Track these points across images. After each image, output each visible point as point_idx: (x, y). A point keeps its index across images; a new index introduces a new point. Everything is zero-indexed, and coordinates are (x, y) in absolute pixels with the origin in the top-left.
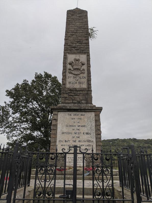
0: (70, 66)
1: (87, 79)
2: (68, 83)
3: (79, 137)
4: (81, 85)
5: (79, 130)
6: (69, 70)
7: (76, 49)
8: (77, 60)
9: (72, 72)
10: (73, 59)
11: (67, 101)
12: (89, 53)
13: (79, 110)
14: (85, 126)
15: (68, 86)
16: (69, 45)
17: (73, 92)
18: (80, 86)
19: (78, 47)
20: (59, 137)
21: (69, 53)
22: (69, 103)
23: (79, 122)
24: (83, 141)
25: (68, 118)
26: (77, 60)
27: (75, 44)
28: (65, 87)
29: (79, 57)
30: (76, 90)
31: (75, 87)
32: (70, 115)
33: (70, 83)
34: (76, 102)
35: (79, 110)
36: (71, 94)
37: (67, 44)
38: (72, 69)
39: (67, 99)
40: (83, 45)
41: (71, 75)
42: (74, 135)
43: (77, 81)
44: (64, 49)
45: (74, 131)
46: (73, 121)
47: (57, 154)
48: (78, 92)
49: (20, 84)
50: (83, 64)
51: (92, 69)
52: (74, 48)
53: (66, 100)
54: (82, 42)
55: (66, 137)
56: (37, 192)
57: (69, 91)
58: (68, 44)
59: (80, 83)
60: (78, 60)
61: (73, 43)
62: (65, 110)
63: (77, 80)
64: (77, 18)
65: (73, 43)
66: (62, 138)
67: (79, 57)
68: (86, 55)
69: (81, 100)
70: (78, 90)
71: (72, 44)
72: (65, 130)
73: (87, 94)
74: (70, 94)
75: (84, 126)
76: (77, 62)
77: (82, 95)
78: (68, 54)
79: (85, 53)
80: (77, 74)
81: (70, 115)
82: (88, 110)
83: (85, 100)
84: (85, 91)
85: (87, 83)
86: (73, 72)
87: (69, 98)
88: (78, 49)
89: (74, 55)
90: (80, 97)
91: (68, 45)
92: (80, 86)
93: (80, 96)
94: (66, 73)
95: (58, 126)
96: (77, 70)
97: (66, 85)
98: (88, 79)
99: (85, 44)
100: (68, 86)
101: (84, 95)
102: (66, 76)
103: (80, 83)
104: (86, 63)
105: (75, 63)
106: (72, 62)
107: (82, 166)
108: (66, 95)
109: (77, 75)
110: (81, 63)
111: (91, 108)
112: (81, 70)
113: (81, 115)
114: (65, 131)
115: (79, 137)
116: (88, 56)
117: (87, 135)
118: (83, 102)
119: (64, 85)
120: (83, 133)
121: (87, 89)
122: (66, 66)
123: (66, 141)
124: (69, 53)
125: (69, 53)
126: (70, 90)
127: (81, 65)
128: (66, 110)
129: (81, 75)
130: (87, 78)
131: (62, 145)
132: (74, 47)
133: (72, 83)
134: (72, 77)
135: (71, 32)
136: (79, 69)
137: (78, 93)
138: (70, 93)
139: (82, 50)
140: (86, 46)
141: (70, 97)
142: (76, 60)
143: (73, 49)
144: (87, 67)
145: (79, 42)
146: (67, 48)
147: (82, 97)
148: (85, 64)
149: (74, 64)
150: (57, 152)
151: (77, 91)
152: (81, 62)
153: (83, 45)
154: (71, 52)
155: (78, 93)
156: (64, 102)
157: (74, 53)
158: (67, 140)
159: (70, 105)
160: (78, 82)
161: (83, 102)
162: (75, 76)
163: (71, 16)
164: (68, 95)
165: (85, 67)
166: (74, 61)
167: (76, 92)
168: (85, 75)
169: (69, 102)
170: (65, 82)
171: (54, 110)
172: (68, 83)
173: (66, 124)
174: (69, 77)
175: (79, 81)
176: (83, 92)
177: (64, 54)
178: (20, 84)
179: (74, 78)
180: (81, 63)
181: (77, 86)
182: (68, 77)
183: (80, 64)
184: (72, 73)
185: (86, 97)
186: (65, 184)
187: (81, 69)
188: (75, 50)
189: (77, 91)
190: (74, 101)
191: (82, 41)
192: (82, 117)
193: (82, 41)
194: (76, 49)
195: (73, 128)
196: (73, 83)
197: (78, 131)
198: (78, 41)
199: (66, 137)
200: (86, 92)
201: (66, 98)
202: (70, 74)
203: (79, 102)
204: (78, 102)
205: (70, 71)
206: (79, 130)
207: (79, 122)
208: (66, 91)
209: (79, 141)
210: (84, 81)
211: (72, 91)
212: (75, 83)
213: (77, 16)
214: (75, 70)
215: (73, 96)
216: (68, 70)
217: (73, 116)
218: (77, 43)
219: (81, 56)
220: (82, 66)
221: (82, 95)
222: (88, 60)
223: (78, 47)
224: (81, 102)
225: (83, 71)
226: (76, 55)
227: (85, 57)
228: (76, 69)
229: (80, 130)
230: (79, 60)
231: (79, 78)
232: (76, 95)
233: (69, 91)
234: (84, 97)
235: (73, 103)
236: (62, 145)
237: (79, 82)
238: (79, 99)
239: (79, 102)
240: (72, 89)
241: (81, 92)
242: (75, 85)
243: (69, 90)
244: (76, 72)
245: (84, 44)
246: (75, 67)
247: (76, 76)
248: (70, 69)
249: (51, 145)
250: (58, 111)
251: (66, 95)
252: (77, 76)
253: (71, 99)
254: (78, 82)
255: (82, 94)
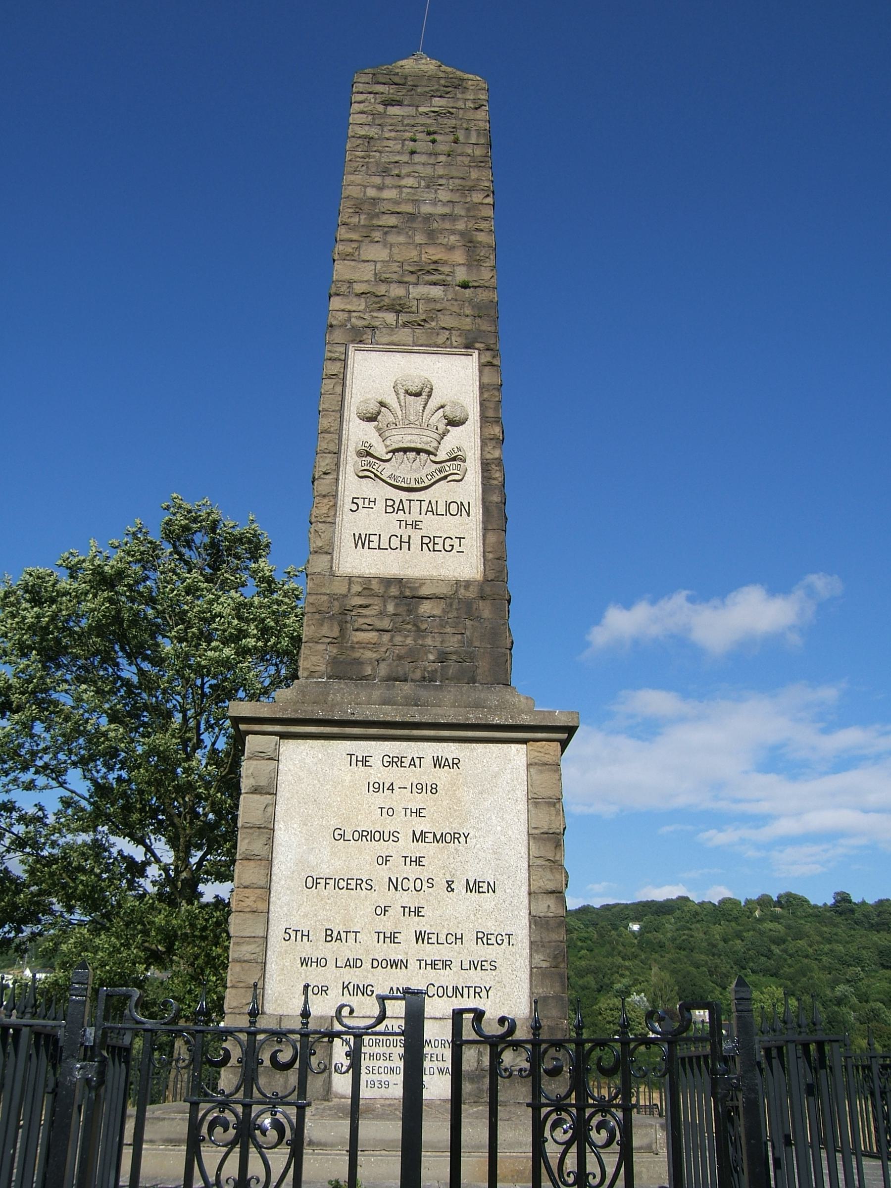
3: (418, 912)
5: (418, 861)
8: (418, 394)
9: (379, 467)
14: (462, 839)
20: (289, 905)
23: (418, 813)
24: (442, 939)
25: (347, 784)
32: (365, 761)
33: (361, 541)
38: (380, 450)
42: (382, 895)
43: (410, 531)
45: (382, 874)
46: (381, 799)
47: (252, 1034)
49: (829, 904)
52: (398, 312)
55: (334, 908)
56: (232, 1144)
60: (422, 392)
63: (415, 525)
64: (422, 120)
66: (305, 915)
72: (331, 860)
75: (455, 837)
81: (365, 761)
95: (281, 835)
106: (382, 404)
112: (442, 455)
113: (438, 763)
114: (325, 871)
115: (418, 912)
117: (474, 895)
120: (449, 884)
123: (335, 935)
127: (442, 427)
129: (440, 493)
131: (304, 962)
134: (381, 504)
136: (428, 453)
149: (391, 419)
150: (253, 1023)
157: (394, 347)
158: (341, 928)
163: (381, 108)
171: (257, 728)
173: (334, 822)
174: (360, 502)
178: (829, 904)
179: (393, 507)
182: (349, 505)
187: (437, 449)
192: (442, 776)
194: (403, 318)
195: (383, 848)
197: (413, 871)
199: (334, 908)
206: (418, 861)
207: (418, 813)
209: (420, 937)
212: (395, 542)
213: (421, 109)
217: (378, 772)
218: (412, 279)
225: (450, 467)
228: (405, 450)
229: (424, 861)
236: (304, 962)
237: (426, 540)
244: (408, 470)
246: (400, 439)
247: (404, 495)
249: (238, 961)
250: (284, 736)
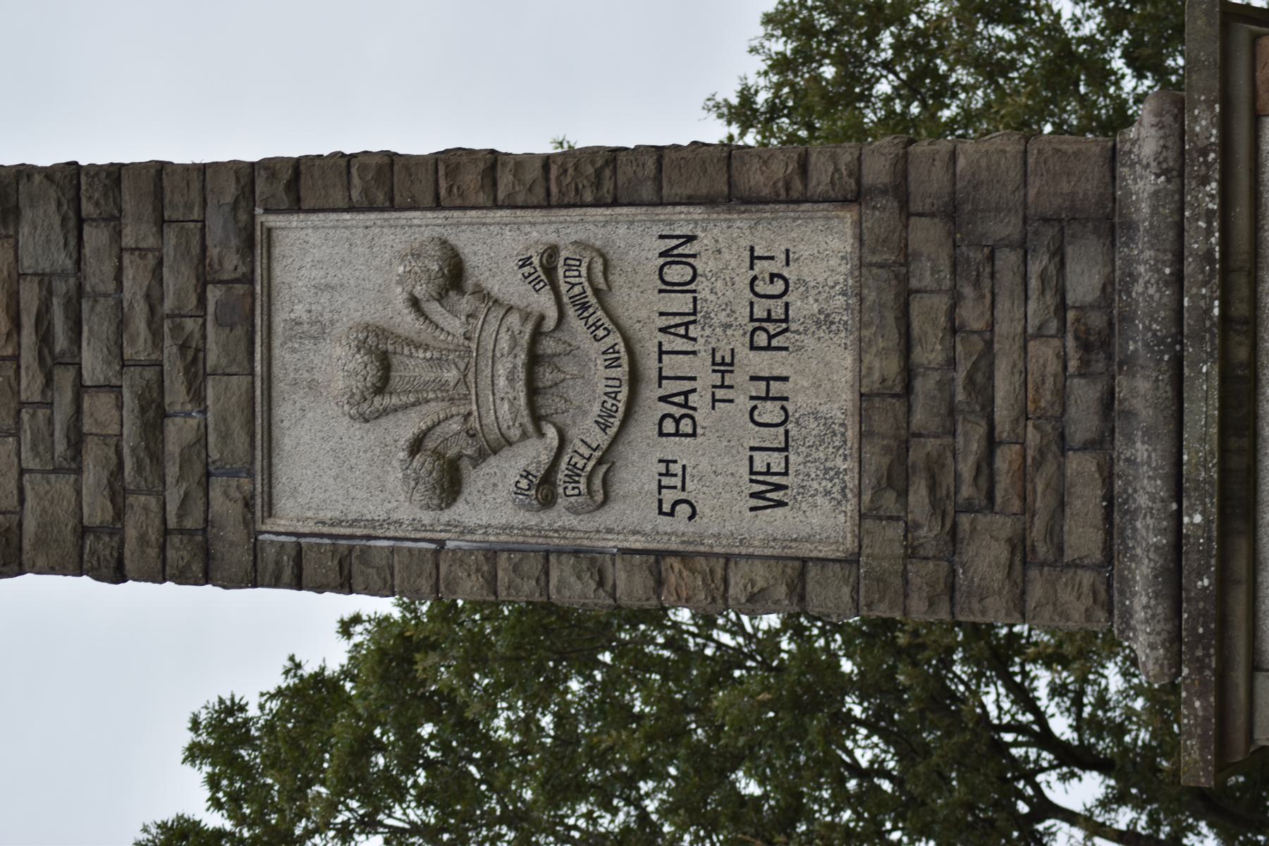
0: (475, 479)
1: (697, 212)
2: (777, 522)
4: (802, 307)
6: (548, 502)
7: (177, 393)
8: (385, 363)
10: (358, 437)
11: (1083, 537)
12: (247, 176)
13: (1242, 354)
15: (820, 518)
16: (117, 493)
17: (931, 445)
18: (824, 321)
19: (139, 346)
21: (255, 506)
22: (1109, 498)
26: (385, 363)
27: (99, 409)
28: (852, 560)
29: (319, 331)
30: (886, 400)
31: (840, 404)
33: (768, 494)
34: (1084, 395)
35: (1242, 354)
36: (966, 469)
37: (83, 531)
39: (1039, 524)
40: (108, 268)
41: (638, 473)
43: (738, 377)
44: (182, 578)
48: (930, 353)
50: (454, 275)
51: (525, 136)
52: (163, 415)
53: (1060, 549)
54: (45, 280)
57: (919, 495)
58: (97, 510)
59: (770, 329)
61: (77, 441)
62: (1240, 566)
63: (724, 366)
65: (77, 441)
67: (319, 331)
68: (295, 220)
69: (1062, 307)
70: (892, 366)
71: (93, 456)
73: (952, 212)
74: (966, 491)
76: (411, 368)
77: (968, 291)
78: (282, 524)
79: (251, 242)
80: (622, 372)
82: (1241, 211)
83: (1059, 255)
84: (906, 256)
85: (767, 212)
86: (588, 433)
87: (1027, 509)
88: (183, 347)
89: (283, 411)
90: (1002, 328)
91: (119, 514)
92: (824, 321)
93: (991, 326)
94: (612, 543)
96: (547, 376)
97: (805, 550)
98: (709, 201)
99: (95, 237)
100: (820, 518)
101: (972, 265)
102: (660, 555)
103: (770, 329)
104: (424, 226)
105: (435, 410)
106: (416, 446)
107: (86, 228)
108: (986, 556)
109: (635, 378)
110: (433, 308)
111: (1205, 181)
112: (544, 302)
116: (298, 183)
118: (1084, 282)
119: (813, 572)
121: (882, 215)
122: (491, 554)
124: (248, 504)
125: (248, 504)
126: (896, 479)
127: (465, 303)
128: (1241, 545)
129: (640, 304)
130: (684, 219)
132: (154, 416)
133: (777, 461)
134: (671, 448)
135: (238, 383)
136: (537, 334)
137: (952, 362)
138: (947, 481)
139: (202, 284)
140: (114, 220)
141: (1004, 482)
142: (382, 386)
143: (178, 433)
144: (496, 206)
145: (61, 342)
146: (166, 532)
147: (1003, 305)
148: (444, 243)
149: (455, 426)
151: (909, 373)
152: (415, 303)
153: (98, 273)
154: (234, 474)
155: (952, 362)
156: (1087, 578)
159: (1146, 490)
160: (763, 363)
161: (1084, 282)
162: (651, 409)
164: (983, 520)
165: (498, 246)
166: (408, 426)
167: (925, 385)
168: (633, 238)
169: (1086, 501)
170: (761, 575)
172: (777, 522)
174: (669, 497)
175: (739, 343)
176: (923, 276)
177: (276, 583)
179: (680, 419)
180: (433, 308)
181: (826, 375)
182: (680, 523)
183: (455, 325)
184: (607, 458)
185: (1008, 227)
186: (939, 291)
188: (197, 396)
189: (909, 373)
190: (1083, 418)
191: (30, 296)
193: (30, 296)
194: (177, 393)
196: (775, 437)
198: (28, 356)
200: (927, 235)
201: (1020, 548)
202: (618, 489)
203: (1099, 345)
204: (1085, 363)
205: (567, 494)
208: (912, 552)
210: (736, 261)
211: (917, 455)
212: (770, 412)
214: (548, 404)
215: (992, 442)
216: (547, 519)
218: (64, 378)
219: (300, 311)
220: (482, 294)
221: (968, 291)
222: (379, 182)
223: (139, 346)
224: (1096, 320)
225: (572, 281)
226: (280, 387)
227: (313, 237)
228: (533, 391)
230: (381, 332)
231: (680, 344)
232: (982, 390)
233: (919, 495)
234: (1008, 260)
235: (1101, 443)
237: (761, 339)
238: (1044, 354)
239: (1085, 346)
240: (877, 460)
241: (928, 313)
242: (800, 403)
243: (889, 501)
244: (589, 384)
245: (78, 262)
246: (503, 403)
247: (650, 392)
248: (544, 489)
251: (986, 556)
252: (650, 365)
253: (1050, 468)
254: (763, 363)
255: (956, 299)
